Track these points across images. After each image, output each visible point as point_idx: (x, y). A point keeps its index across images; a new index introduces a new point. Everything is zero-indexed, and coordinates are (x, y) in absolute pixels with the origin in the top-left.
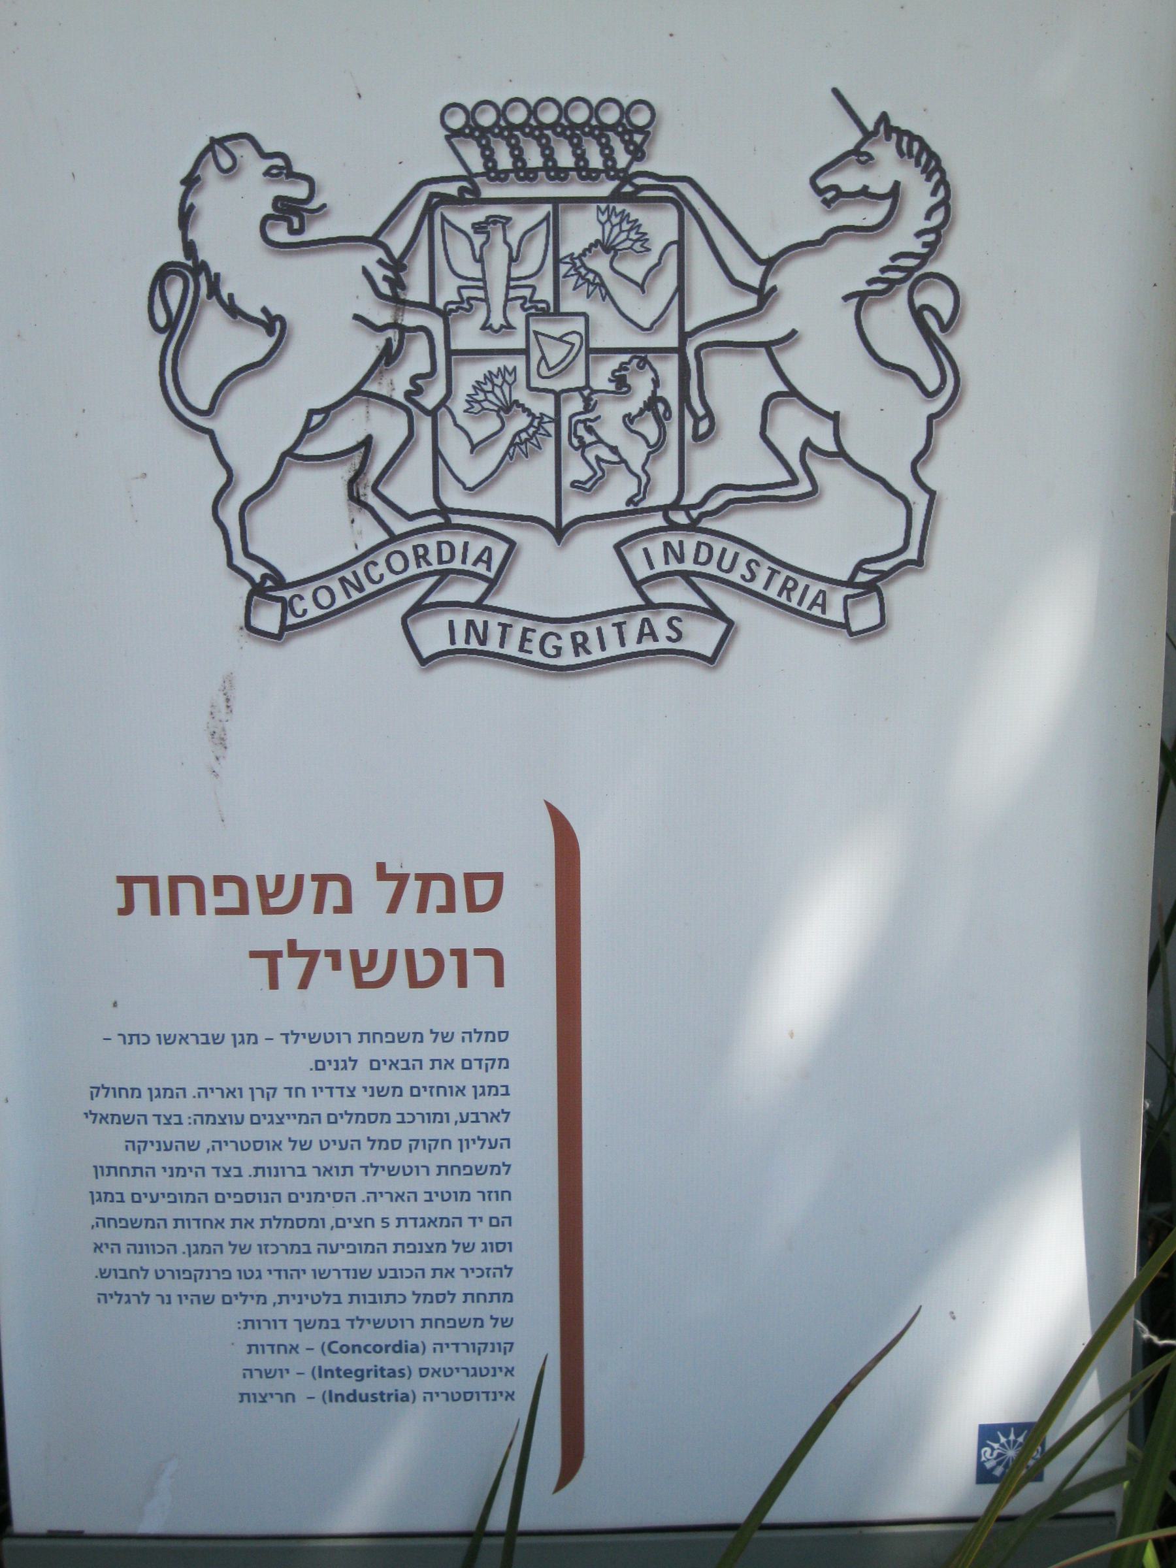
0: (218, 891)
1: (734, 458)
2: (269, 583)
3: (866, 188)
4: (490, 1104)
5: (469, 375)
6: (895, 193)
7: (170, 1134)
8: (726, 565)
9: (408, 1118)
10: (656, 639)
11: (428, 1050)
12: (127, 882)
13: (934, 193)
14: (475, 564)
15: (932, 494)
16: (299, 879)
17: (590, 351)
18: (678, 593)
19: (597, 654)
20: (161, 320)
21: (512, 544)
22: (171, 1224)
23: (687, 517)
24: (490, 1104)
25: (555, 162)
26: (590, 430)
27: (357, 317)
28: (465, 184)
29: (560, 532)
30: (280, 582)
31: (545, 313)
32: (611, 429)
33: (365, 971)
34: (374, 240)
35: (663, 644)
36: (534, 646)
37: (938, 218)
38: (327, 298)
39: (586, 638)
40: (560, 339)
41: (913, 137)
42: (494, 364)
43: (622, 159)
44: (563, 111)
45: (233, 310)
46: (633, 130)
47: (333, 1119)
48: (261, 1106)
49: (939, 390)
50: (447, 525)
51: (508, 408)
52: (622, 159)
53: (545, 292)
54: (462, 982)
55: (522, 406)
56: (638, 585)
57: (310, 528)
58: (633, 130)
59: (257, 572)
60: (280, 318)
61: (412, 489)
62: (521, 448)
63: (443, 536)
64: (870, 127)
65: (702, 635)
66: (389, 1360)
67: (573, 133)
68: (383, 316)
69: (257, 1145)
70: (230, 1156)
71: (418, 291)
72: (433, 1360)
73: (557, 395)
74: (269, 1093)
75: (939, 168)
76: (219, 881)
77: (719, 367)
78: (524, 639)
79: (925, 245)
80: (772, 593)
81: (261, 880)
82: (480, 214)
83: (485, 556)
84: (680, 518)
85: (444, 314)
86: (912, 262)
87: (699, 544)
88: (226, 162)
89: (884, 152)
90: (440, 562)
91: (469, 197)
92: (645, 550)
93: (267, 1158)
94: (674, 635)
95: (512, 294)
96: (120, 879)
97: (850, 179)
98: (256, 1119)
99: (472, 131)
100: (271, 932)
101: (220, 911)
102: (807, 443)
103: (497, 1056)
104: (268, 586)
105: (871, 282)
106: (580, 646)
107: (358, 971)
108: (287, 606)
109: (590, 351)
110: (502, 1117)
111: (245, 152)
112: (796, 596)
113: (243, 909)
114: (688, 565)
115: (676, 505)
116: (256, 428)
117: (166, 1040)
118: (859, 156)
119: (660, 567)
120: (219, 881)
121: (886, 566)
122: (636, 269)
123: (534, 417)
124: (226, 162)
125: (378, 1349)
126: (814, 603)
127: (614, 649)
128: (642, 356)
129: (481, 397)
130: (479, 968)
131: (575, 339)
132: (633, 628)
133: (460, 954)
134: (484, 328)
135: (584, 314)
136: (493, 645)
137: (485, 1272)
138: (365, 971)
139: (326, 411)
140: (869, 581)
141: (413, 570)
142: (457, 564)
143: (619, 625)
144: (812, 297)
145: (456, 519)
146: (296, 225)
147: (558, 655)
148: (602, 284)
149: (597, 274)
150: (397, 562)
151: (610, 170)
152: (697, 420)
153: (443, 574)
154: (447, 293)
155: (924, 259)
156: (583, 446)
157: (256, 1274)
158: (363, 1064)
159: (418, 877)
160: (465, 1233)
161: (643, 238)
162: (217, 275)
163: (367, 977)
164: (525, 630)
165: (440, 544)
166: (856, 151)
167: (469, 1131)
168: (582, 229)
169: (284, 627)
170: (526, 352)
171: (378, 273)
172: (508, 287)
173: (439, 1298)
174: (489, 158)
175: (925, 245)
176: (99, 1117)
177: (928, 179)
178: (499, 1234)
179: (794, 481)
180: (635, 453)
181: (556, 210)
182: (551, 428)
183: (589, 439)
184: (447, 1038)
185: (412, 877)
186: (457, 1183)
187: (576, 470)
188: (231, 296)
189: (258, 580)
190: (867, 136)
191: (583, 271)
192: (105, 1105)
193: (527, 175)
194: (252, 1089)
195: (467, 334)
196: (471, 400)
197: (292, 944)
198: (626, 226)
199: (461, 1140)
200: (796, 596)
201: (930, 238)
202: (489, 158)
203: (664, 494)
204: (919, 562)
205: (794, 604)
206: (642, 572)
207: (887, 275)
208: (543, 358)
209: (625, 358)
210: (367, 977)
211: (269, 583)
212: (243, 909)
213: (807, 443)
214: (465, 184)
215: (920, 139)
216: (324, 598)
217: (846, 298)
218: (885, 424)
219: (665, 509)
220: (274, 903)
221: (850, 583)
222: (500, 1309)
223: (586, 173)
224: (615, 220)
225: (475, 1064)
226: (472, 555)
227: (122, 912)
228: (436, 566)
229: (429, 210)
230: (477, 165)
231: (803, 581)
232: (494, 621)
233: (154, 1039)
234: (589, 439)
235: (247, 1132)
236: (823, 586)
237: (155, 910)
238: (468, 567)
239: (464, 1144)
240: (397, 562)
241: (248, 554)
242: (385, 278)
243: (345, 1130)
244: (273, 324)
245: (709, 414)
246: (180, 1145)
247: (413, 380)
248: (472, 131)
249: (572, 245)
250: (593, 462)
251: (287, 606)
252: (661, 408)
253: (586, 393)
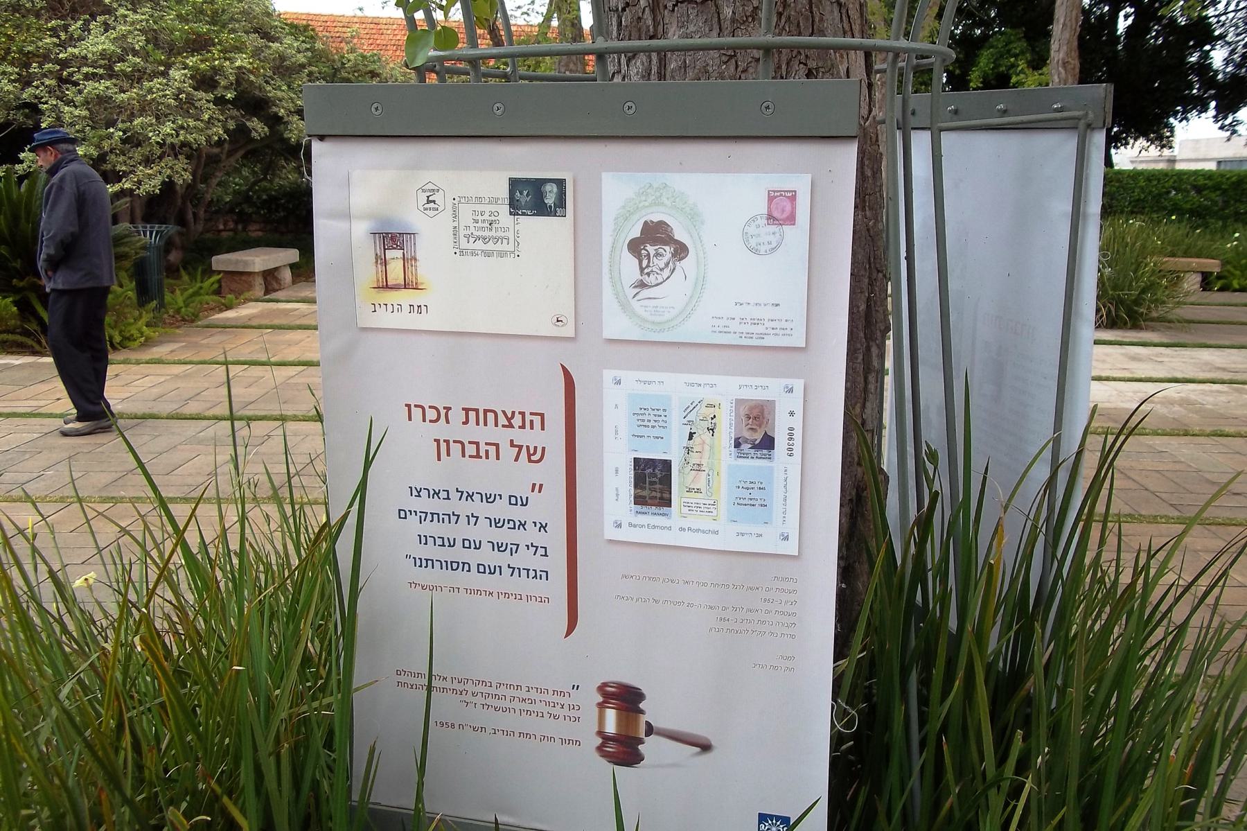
12: (467, 410)
22: (517, 735)
100: (441, 430)
133: (447, 442)
163: (533, 458)
176: (465, 495)
194: (408, 406)
199: (437, 441)
210: (533, 458)
237: (478, 424)
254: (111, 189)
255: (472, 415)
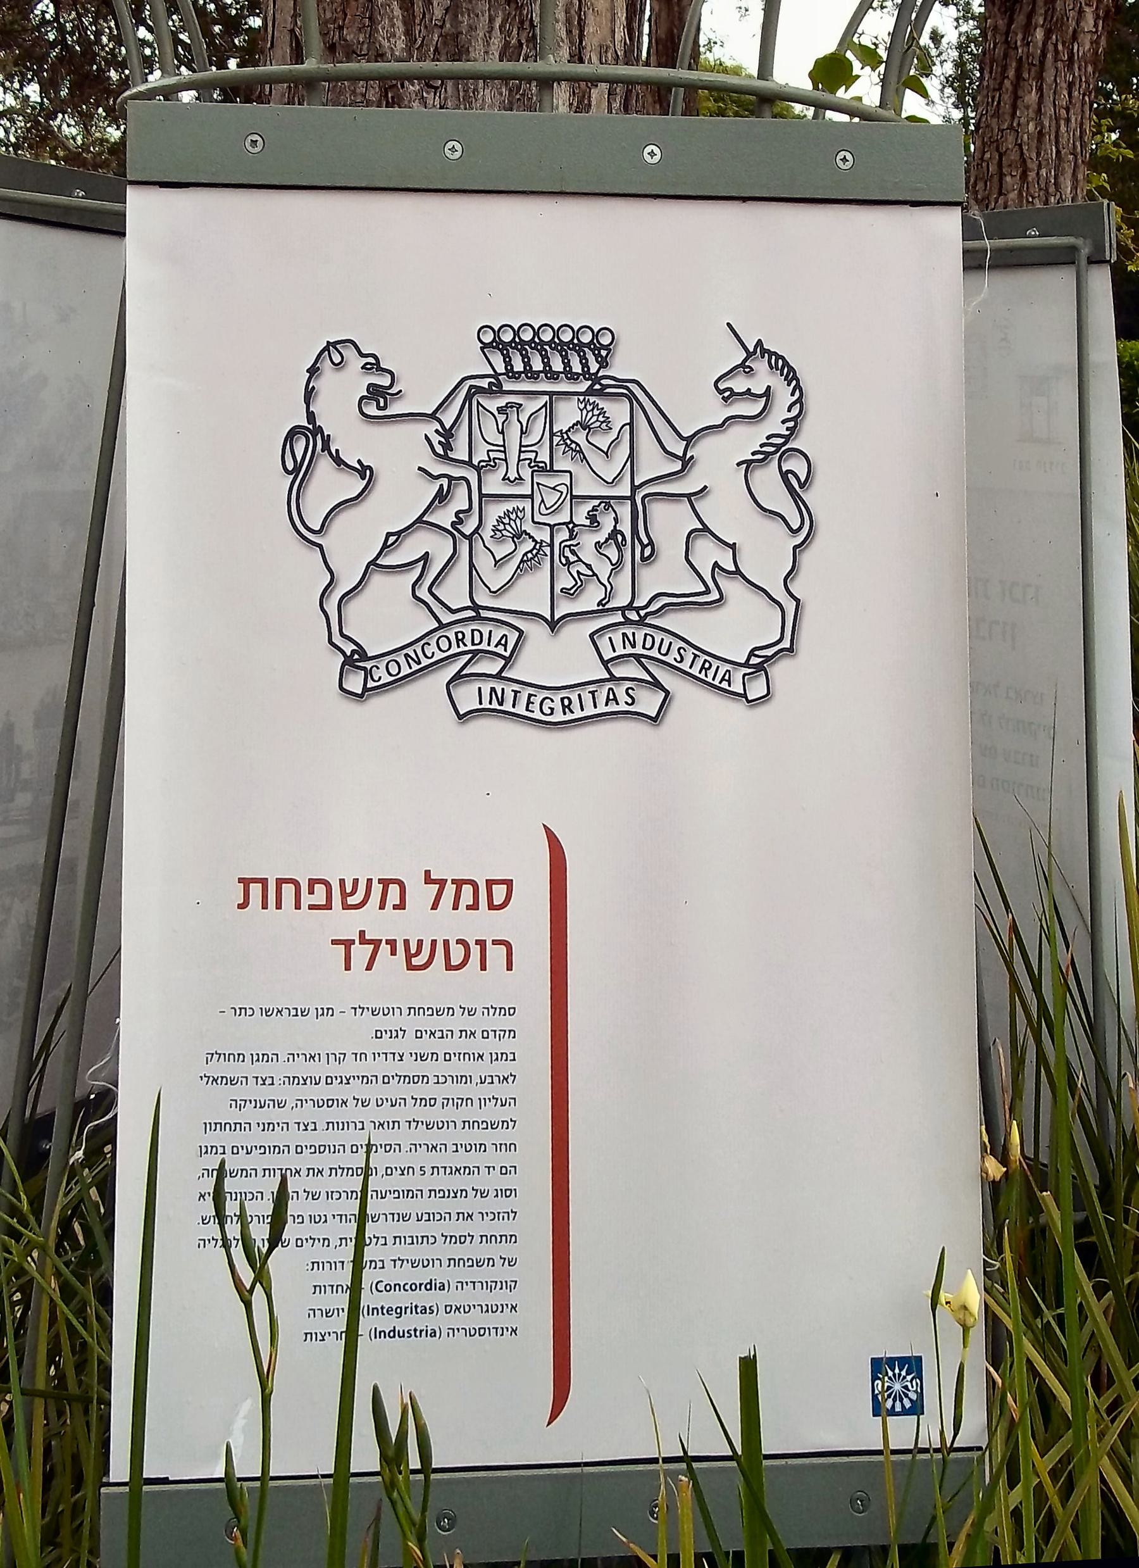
0: (311, 892)
1: (668, 575)
2: (356, 656)
3: (749, 389)
4: (502, 1068)
5: (495, 512)
6: (768, 393)
7: (264, 1093)
8: (664, 651)
9: (442, 1080)
10: (617, 704)
11: (458, 1022)
12: (246, 882)
13: (793, 394)
14: (496, 646)
15: (797, 601)
16: (370, 881)
17: (573, 497)
18: (631, 670)
19: (578, 714)
20: (290, 466)
21: (521, 632)
23: (638, 616)
24: (502, 1068)
25: (550, 367)
26: (573, 553)
27: (420, 469)
28: (492, 380)
29: (554, 625)
30: (364, 657)
31: (543, 470)
32: (588, 554)
33: (414, 957)
34: (433, 416)
35: (623, 707)
36: (536, 707)
37: (795, 411)
38: (401, 457)
39: (570, 702)
40: (554, 488)
41: (779, 357)
42: (510, 506)
43: (594, 367)
44: (556, 333)
45: (338, 460)
46: (601, 348)
47: (386, 1079)
48: (334, 1069)
49: (800, 528)
50: (478, 618)
51: (518, 536)
52: (594, 367)
53: (544, 457)
54: (483, 967)
55: (527, 534)
56: (605, 663)
57: (387, 618)
58: (601, 348)
59: (349, 648)
60: (370, 468)
61: (455, 591)
62: (528, 564)
63: (475, 626)
64: (751, 350)
65: (649, 703)
66: (423, 1298)
67: (562, 348)
68: (437, 469)
69: (330, 1103)
70: (308, 1113)
71: (461, 453)
72: (454, 1297)
73: (552, 527)
74: (340, 1058)
75: (795, 378)
76: (312, 883)
77: (659, 512)
78: (529, 702)
79: (788, 429)
80: (695, 671)
81: (342, 882)
82: (502, 402)
83: (503, 642)
84: (633, 616)
85: (478, 469)
86: (780, 441)
87: (646, 635)
88: (337, 358)
89: (761, 366)
90: (473, 644)
91: (495, 389)
92: (610, 638)
93: (335, 1114)
94: (630, 701)
95: (523, 456)
96: (240, 880)
97: (739, 384)
98: (329, 1081)
99: (497, 344)
100: (347, 923)
101: (312, 907)
102: (716, 565)
103: (507, 1029)
104: (356, 659)
105: (753, 454)
106: (567, 708)
107: (409, 957)
108: (368, 674)
109: (573, 497)
110: (511, 1079)
111: (350, 353)
112: (711, 673)
113: (328, 906)
114: (639, 650)
115: (630, 607)
116: (353, 543)
117: (267, 1013)
118: (744, 368)
119: (620, 651)
120: (312, 883)
121: (769, 652)
122: (603, 442)
123: (537, 543)
124: (337, 358)
125: (414, 1287)
126: (723, 679)
127: (590, 711)
128: (607, 502)
129: (501, 527)
130: (496, 955)
131: (563, 489)
132: (602, 696)
133: (481, 943)
134: (503, 479)
135: (570, 472)
136: (508, 707)
137: (496, 1216)
138: (414, 957)
139: (398, 534)
140: (759, 664)
141: (455, 650)
142: (484, 646)
143: (593, 693)
144: (718, 460)
145: (484, 613)
146: (382, 404)
147: (552, 714)
148: (581, 451)
149: (577, 444)
150: (444, 644)
151: (586, 374)
152: (643, 547)
153: (475, 653)
154: (480, 456)
155: (787, 439)
156: (569, 563)
157: (323, 1219)
158: (411, 1034)
159: (453, 881)
160: (481, 1181)
161: (607, 420)
162: (329, 436)
163: (415, 961)
164: (530, 696)
165: (473, 631)
166: (743, 365)
167: (487, 1091)
168: (568, 414)
169: (365, 689)
170: (531, 497)
171: (436, 439)
172: (520, 452)
173: (461, 1240)
174: (508, 363)
175: (788, 429)
177: (789, 385)
178: (507, 1182)
179: (708, 591)
180: (603, 570)
181: (551, 399)
182: (547, 550)
183: (573, 558)
184: (471, 1012)
185: (449, 882)
186: (476, 1136)
187: (565, 581)
188: (337, 451)
189: (349, 654)
190: (749, 355)
191: (568, 442)
192: (218, 1068)
193: (533, 376)
195: (494, 484)
196: (495, 529)
197: (362, 933)
198: (596, 412)
200: (711, 673)
201: (792, 424)
202: (508, 363)
203: (622, 600)
204: (791, 649)
205: (710, 679)
206: (608, 654)
207: (764, 449)
208: (543, 501)
209: (597, 502)
210: (415, 961)
211: (356, 656)
212: (328, 906)
213: (716, 565)
214: (492, 380)
215: (783, 358)
216: (394, 669)
217: (739, 464)
218: (766, 553)
219: (623, 609)
220: (351, 901)
221: (746, 665)
222: (506, 1250)
223: (573, 377)
224: (589, 408)
225: (491, 1034)
226: (494, 641)
227: (241, 906)
228: (470, 647)
229: (469, 397)
230: (501, 368)
231: (715, 663)
232: (509, 689)
233: (257, 1012)
234: (573, 558)
235: (322, 1092)
236: (728, 667)
237: (265, 906)
238: (492, 648)
239: (483, 1102)
240: (444, 644)
241: (342, 635)
242: (440, 442)
243: (396, 1090)
244: (364, 471)
245: (651, 543)
246: (271, 1103)
247: (457, 514)
248: (497, 344)
249: (561, 425)
250: (576, 575)
251: (368, 674)
252: (620, 538)
253: (571, 526)
254: (448, 25)
255: (256, 889)
